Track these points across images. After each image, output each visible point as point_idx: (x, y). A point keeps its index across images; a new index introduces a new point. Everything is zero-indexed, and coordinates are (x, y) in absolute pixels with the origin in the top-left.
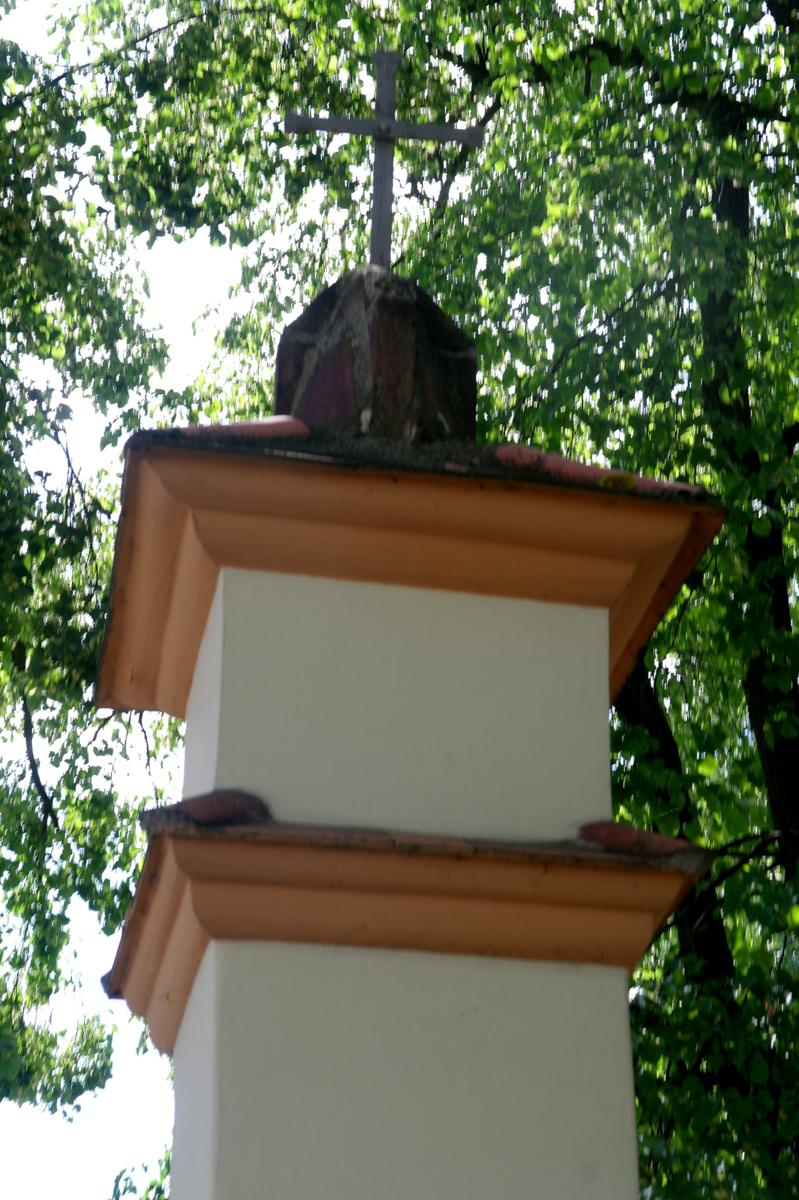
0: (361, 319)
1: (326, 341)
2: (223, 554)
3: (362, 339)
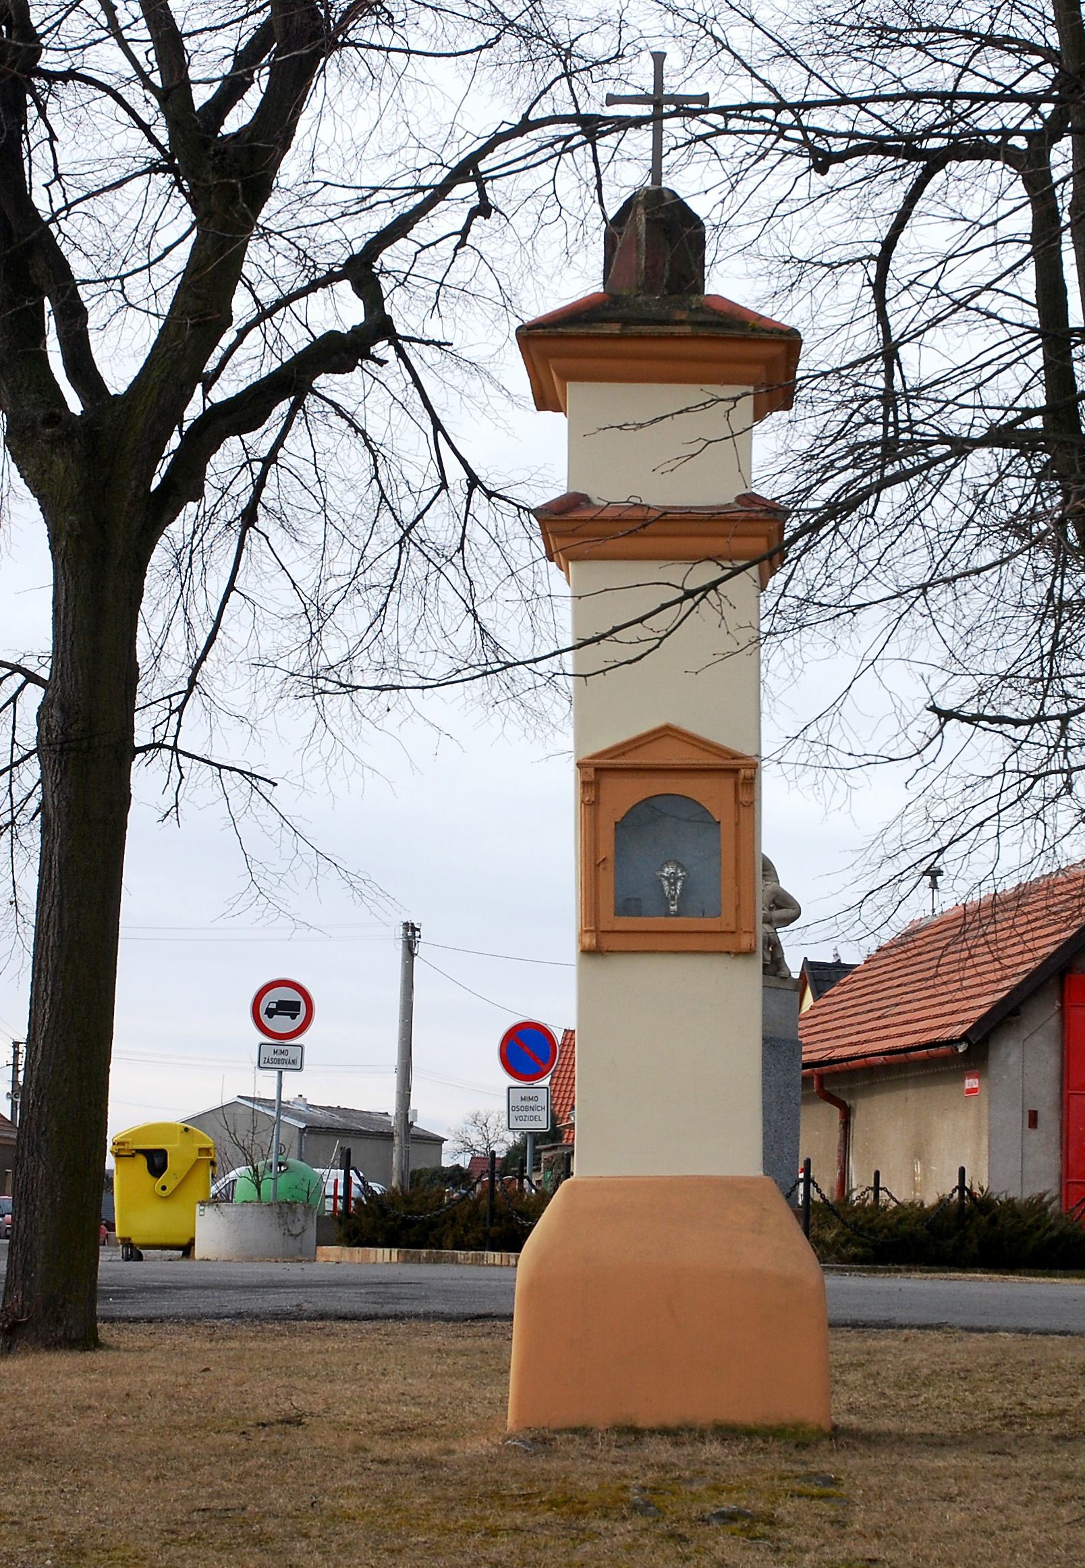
0: (641, 216)
1: (626, 230)
2: (567, 377)
3: (642, 229)
